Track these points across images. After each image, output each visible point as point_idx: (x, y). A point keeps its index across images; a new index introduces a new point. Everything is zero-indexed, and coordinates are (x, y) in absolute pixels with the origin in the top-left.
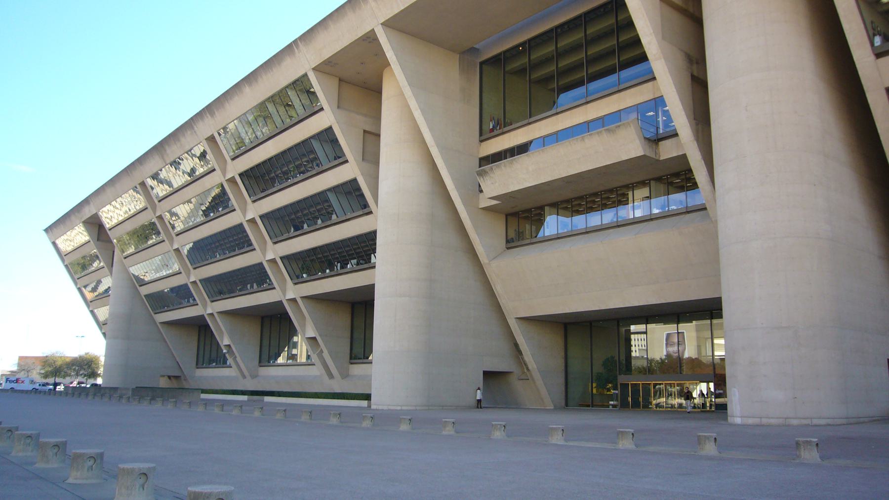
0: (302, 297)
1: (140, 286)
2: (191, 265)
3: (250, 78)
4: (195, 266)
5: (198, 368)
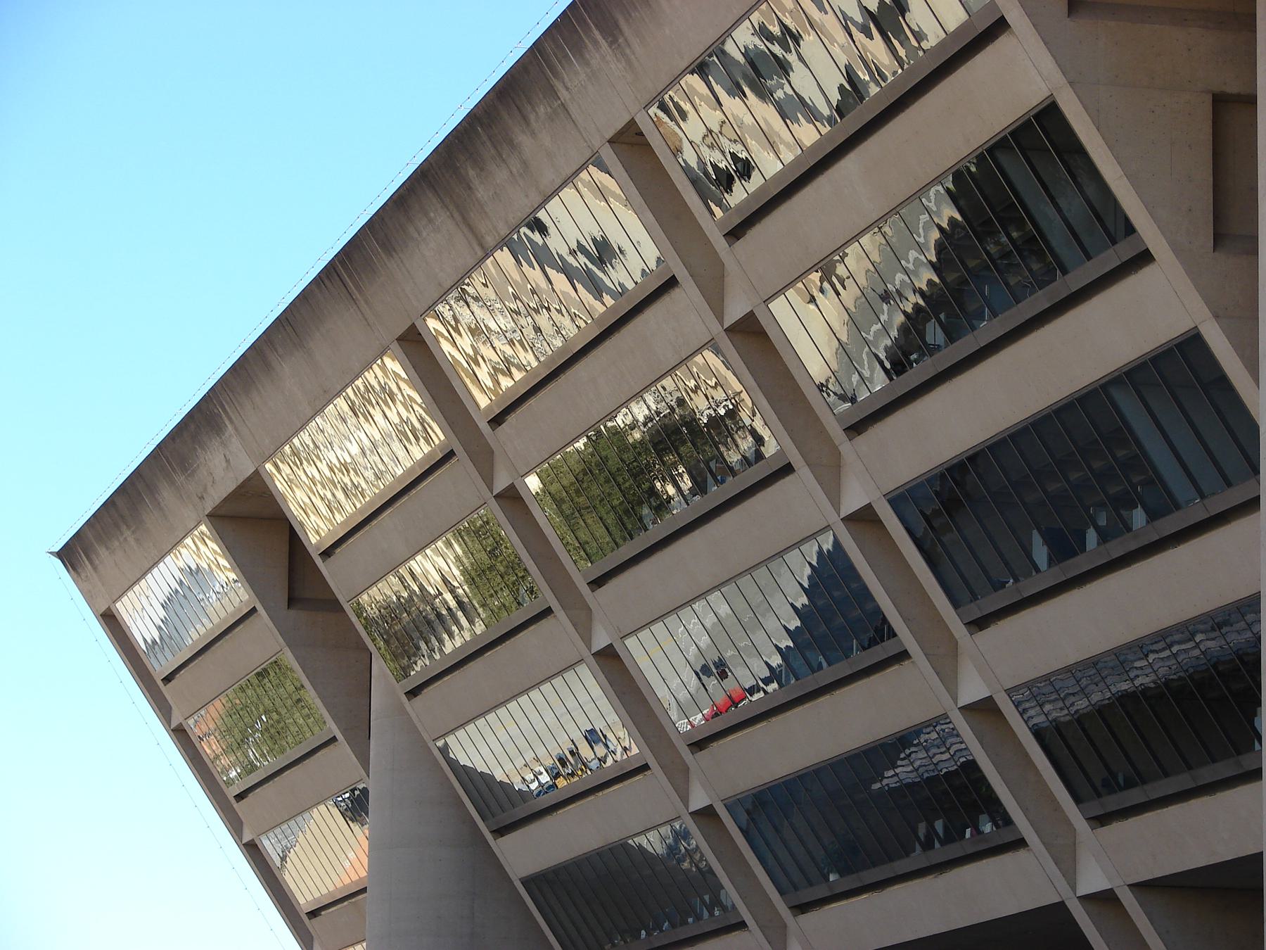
1: (500, 832)
2: (956, 604)
4: (976, 612)
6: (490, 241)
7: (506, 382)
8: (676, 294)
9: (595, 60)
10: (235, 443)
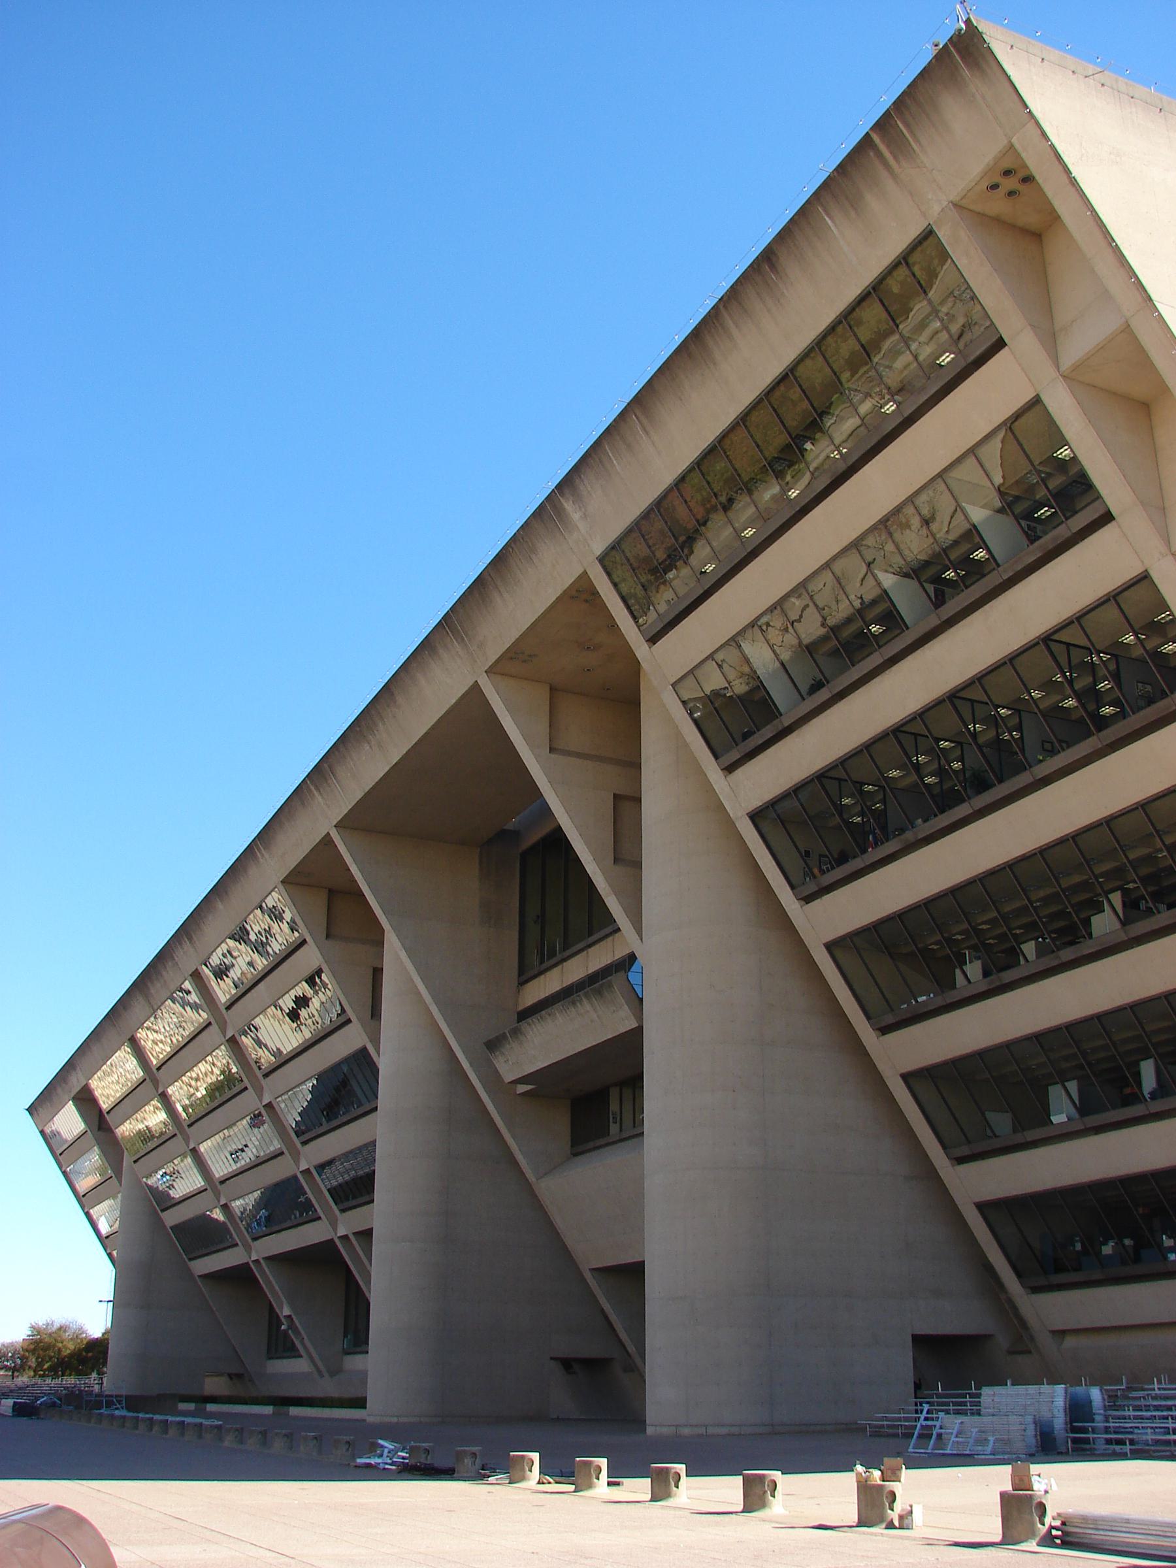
0: (354, 1233)
1: (163, 1210)
3: (320, 774)
5: (270, 1358)
6: (155, 1007)
7: (161, 1056)
8: (211, 1027)
9: (186, 948)
10: (80, 1074)
